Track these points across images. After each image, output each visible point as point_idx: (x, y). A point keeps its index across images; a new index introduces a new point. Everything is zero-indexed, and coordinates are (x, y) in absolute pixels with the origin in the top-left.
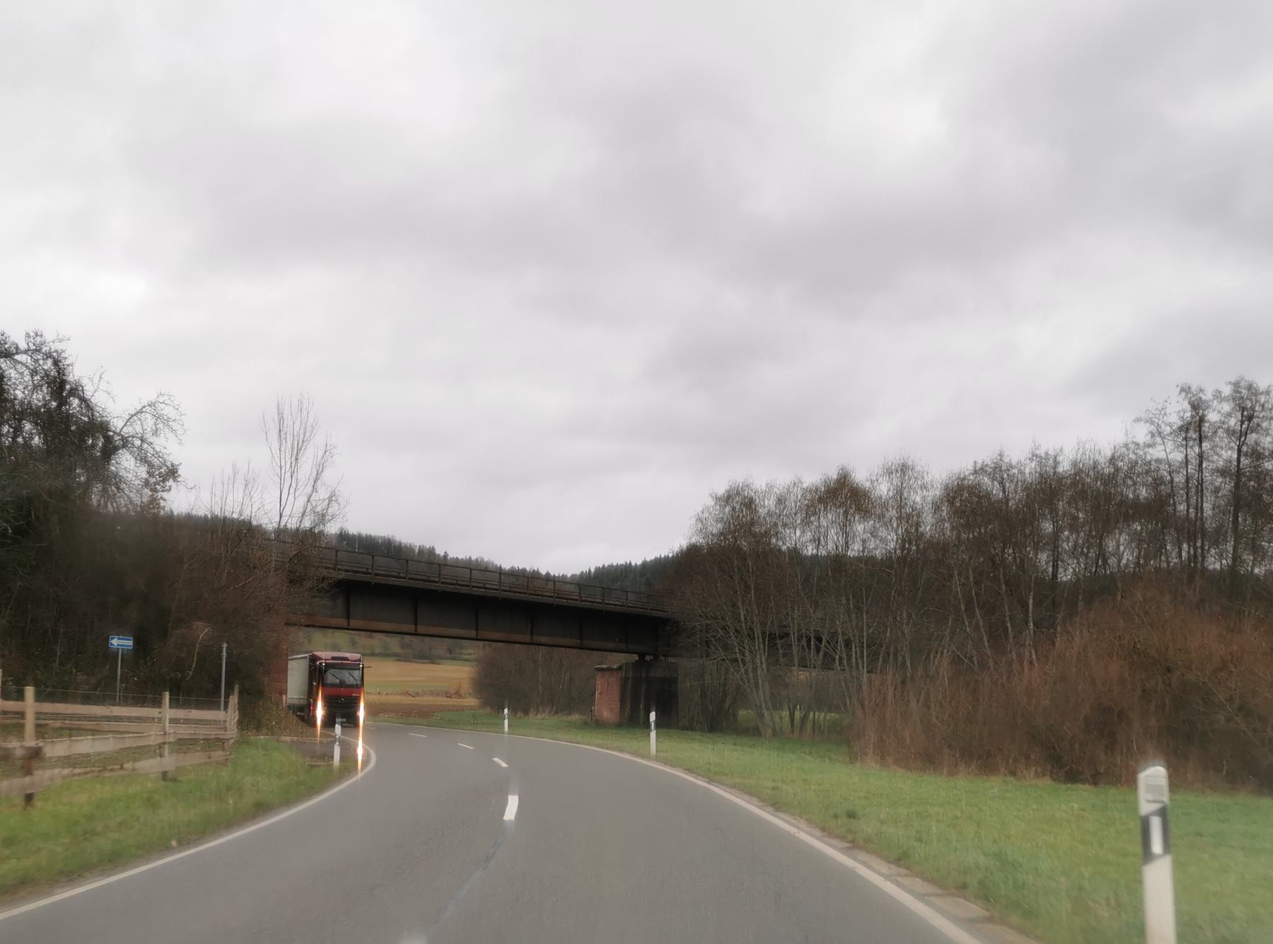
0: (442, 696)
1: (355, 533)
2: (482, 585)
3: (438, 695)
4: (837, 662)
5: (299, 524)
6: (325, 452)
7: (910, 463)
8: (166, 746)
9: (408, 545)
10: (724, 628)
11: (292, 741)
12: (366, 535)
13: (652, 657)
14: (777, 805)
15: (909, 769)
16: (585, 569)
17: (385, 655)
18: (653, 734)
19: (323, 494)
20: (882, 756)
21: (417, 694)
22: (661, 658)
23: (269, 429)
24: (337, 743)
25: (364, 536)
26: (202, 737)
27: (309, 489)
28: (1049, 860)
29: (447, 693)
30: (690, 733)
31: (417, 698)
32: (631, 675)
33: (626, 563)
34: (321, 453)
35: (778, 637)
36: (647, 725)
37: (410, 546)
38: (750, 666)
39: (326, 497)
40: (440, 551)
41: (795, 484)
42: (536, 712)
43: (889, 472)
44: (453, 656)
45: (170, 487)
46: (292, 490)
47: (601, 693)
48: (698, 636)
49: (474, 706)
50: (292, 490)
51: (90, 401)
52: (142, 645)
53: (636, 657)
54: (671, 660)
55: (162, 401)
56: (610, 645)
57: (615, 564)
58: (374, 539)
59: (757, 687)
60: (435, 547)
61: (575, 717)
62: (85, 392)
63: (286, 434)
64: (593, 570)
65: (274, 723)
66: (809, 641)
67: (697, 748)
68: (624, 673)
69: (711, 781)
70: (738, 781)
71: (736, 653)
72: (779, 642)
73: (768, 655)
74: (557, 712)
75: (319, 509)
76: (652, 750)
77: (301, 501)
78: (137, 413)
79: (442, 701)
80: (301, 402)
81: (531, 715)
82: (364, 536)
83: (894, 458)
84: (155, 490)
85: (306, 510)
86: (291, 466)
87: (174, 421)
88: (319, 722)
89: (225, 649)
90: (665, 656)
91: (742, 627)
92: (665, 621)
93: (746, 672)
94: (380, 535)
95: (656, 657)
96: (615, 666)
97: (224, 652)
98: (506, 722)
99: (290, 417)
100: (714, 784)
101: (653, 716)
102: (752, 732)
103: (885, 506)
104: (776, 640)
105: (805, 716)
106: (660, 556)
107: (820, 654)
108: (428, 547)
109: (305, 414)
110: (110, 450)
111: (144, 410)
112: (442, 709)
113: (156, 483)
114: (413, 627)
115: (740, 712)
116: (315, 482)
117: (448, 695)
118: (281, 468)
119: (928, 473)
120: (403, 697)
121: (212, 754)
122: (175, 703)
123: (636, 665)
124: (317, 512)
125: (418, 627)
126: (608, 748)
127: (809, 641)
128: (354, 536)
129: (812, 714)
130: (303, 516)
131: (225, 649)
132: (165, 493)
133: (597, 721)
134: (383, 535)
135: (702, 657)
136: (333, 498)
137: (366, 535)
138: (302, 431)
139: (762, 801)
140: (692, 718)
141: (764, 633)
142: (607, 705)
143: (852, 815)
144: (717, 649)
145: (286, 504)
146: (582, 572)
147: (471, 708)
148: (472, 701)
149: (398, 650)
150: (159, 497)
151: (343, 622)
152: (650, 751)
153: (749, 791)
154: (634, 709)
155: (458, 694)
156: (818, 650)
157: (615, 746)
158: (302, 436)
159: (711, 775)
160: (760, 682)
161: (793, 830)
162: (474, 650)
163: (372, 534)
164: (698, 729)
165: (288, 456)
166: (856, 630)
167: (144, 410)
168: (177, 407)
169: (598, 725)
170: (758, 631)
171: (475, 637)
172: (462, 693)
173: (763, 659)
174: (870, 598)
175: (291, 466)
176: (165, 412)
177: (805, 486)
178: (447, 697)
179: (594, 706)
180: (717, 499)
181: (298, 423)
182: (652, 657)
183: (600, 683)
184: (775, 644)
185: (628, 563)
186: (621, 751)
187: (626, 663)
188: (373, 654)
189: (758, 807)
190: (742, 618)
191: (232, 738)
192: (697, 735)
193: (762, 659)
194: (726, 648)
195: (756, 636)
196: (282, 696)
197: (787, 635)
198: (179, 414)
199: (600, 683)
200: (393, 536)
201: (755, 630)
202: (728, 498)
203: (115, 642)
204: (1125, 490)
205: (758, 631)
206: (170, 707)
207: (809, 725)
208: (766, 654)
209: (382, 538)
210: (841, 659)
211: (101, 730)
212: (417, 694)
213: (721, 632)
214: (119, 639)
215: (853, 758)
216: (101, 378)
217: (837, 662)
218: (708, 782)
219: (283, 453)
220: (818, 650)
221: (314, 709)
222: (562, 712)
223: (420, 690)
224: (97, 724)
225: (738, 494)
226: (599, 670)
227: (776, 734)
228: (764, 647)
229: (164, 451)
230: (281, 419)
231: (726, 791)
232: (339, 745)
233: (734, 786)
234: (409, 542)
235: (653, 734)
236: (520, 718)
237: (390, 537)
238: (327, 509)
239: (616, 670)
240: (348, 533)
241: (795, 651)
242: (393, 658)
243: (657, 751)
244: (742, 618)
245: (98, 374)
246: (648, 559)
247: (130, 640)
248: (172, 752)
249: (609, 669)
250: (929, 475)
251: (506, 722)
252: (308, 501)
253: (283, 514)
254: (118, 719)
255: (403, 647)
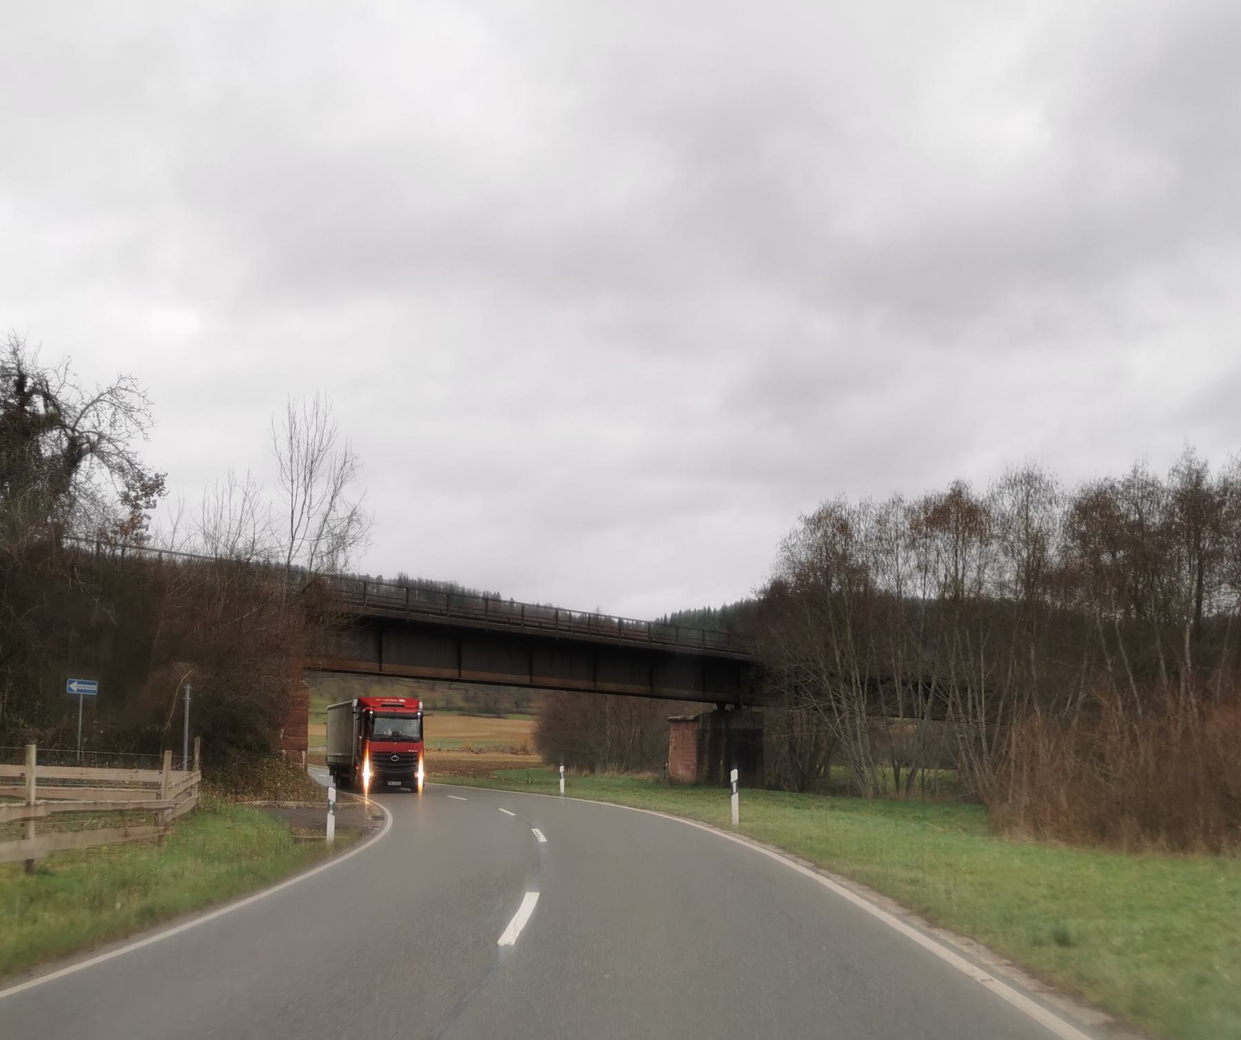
0: (507, 753)
1: (416, 578)
2: (537, 624)
3: (503, 751)
4: (950, 708)
5: (313, 548)
6: (345, 463)
7: (1036, 473)
8: (32, 826)
9: (472, 592)
10: (815, 672)
11: (298, 807)
12: (427, 581)
13: (733, 706)
14: (931, 917)
15: (1071, 841)
16: (661, 616)
17: (448, 708)
18: (735, 798)
19: (342, 512)
20: (1037, 828)
21: (481, 751)
22: (744, 707)
23: (279, 435)
24: (331, 811)
25: (425, 582)
26: (131, 807)
27: (326, 507)
28: (324, 609)
29: (512, 749)
30: (778, 793)
31: (481, 755)
32: (708, 728)
33: (705, 608)
34: (338, 466)
35: (879, 682)
36: (728, 785)
37: (474, 592)
38: (846, 714)
39: (346, 516)
40: (505, 597)
41: (894, 503)
42: (412, 768)
43: (1013, 484)
44: (519, 709)
45: (155, 501)
46: (306, 509)
47: (675, 747)
48: (786, 683)
49: (538, 763)
50: (306, 509)
51: (57, 399)
52: (112, 691)
53: (715, 707)
54: (755, 709)
55: (124, 388)
56: (685, 693)
57: (692, 610)
58: (435, 585)
59: (855, 738)
60: (500, 594)
61: (647, 775)
62: (50, 387)
63: (298, 442)
64: (669, 617)
65: (279, 784)
66: (915, 686)
67: (792, 815)
68: (701, 724)
69: (817, 867)
70: (857, 867)
71: (830, 701)
72: (880, 687)
73: (867, 704)
74: (627, 769)
75: (337, 531)
76: (733, 819)
77: (316, 522)
78: (94, 402)
79: (509, 757)
80: (317, 405)
81: (597, 773)
82: (425, 582)
83: (1018, 466)
84: (136, 507)
85: (322, 530)
86: (305, 479)
87: (139, 410)
88: (366, 783)
89: (188, 692)
90: (748, 705)
91: (837, 670)
92: (745, 665)
93: (842, 722)
94: (442, 581)
95: (738, 706)
96: (691, 717)
97: (188, 696)
98: (562, 781)
99: (303, 422)
100: (823, 871)
101: (734, 775)
102: (846, 792)
103: (1006, 523)
104: (875, 687)
105: (911, 774)
106: (741, 601)
107: (930, 700)
108: (493, 593)
109: (321, 418)
110: (74, 454)
111: (102, 398)
112: (505, 766)
113: (137, 498)
114: (456, 671)
115: (833, 768)
116: (332, 499)
117: (514, 752)
118: (292, 481)
119: (1057, 483)
120: (465, 754)
121: (131, 830)
122: (42, 759)
123: (714, 715)
124: (336, 535)
125: (462, 671)
126: (679, 815)
127: (915, 686)
128: (413, 582)
129: (920, 771)
130: (318, 539)
131: (188, 692)
132: (150, 509)
133: (670, 779)
134: (445, 581)
135: (791, 704)
136: (354, 518)
137: (427, 581)
138: (317, 439)
139: (901, 905)
140: (779, 776)
141: (863, 677)
142: (682, 764)
143: (1063, 940)
144: (809, 697)
145: (299, 525)
146: (658, 619)
147: (536, 765)
148: (536, 758)
149: (462, 704)
150: (142, 515)
151: (374, 666)
152: (731, 820)
153: (877, 885)
154: (713, 768)
155: (524, 750)
156: (926, 696)
157: (687, 811)
158: (317, 444)
159: (820, 858)
160: (859, 733)
161: (979, 975)
162: (540, 700)
163: (433, 580)
164: (785, 787)
165: (301, 468)
166: (974, 672)
167: (102, 398)
168: (143, 394)
169: (673, 784)
170: (856, 675)
171: (528, 683)
172: (529, 750)
173: (863, 707)
174: (989, 634)
175: (305, 479)
176: (127, 400)
177: (906, 505)
178: (512, 753)
179: (668, 762)
180: (809, 521)
181: (313, 429)
182: (733, 706)
183: (674, 736)
184: (877, 690)
185: (707, 608)
186: (695, 818)
187: (703, 714)
188: (435, 708)
189: (898, 916)
190: (838, 660)
191: (168, 808)
192: (786, 796)
193: (861, 706)
194: (818, 694)
195: (853, 680)
196: (301, 753)
197: (890, 679)
198: (146, 403)
199: (674, 736)
200: (455, 582)
201: (852, 674)
202: (816, 522)
203: (74, 686)
204: (1207, 545)
205: (856, 675)
206: (38, 763)
207: (917, 783)
208: (866, 701)
209: (443, 583)
210: (954, 704)
211: (18, 795)
212: (481, 751)
213: (813, 677)
214: (78, 683)
215: (996, 829)
216: (66, 369)
217: (950, 708)
218: (812, 869)
219: (295, 464)
220: (926, 696)
221: (361, 770)
222: (632, 769)
223: (483, 746)
224: (14, 789)
225: (829, 515)
226: (671, 721)
227: (877, 794)
228: (863, 692)
229: (128, 449)
230: (293, 423)
231: (841, 885)
232: (333, 814)
233: (851, 877)
234: (473, 588)
235: (735, 798)
236: (585, 776)
237: (453, 582)
238: (347, 531)
239: (692, 720)
240: (407, 579)
241: (899, 699)
242: (455, 712)
243: (740, 820)
244: (838, 660)
245: (65, 365)
246: (728, 604)
247: (95, 684)
248: (39, 832)
249: (685, 721)
250: (1060, 485)
251: (562, 781)
252: (325, 520)
253: (296, 538)
254: (92, 783)
255: (467, 700)
